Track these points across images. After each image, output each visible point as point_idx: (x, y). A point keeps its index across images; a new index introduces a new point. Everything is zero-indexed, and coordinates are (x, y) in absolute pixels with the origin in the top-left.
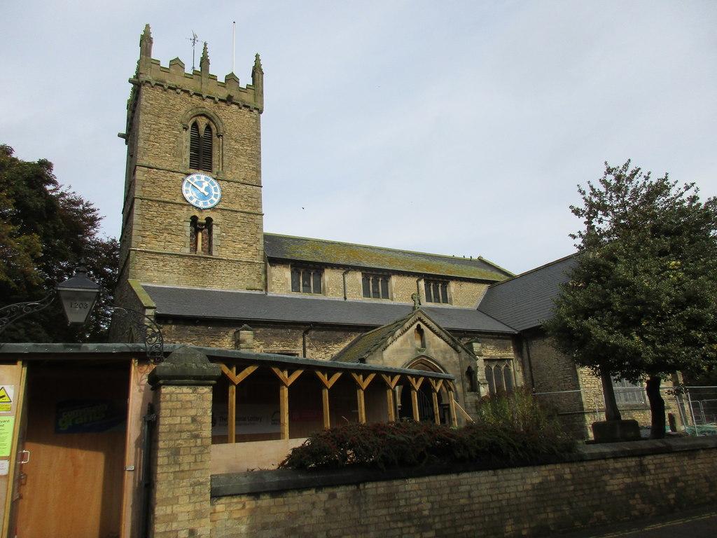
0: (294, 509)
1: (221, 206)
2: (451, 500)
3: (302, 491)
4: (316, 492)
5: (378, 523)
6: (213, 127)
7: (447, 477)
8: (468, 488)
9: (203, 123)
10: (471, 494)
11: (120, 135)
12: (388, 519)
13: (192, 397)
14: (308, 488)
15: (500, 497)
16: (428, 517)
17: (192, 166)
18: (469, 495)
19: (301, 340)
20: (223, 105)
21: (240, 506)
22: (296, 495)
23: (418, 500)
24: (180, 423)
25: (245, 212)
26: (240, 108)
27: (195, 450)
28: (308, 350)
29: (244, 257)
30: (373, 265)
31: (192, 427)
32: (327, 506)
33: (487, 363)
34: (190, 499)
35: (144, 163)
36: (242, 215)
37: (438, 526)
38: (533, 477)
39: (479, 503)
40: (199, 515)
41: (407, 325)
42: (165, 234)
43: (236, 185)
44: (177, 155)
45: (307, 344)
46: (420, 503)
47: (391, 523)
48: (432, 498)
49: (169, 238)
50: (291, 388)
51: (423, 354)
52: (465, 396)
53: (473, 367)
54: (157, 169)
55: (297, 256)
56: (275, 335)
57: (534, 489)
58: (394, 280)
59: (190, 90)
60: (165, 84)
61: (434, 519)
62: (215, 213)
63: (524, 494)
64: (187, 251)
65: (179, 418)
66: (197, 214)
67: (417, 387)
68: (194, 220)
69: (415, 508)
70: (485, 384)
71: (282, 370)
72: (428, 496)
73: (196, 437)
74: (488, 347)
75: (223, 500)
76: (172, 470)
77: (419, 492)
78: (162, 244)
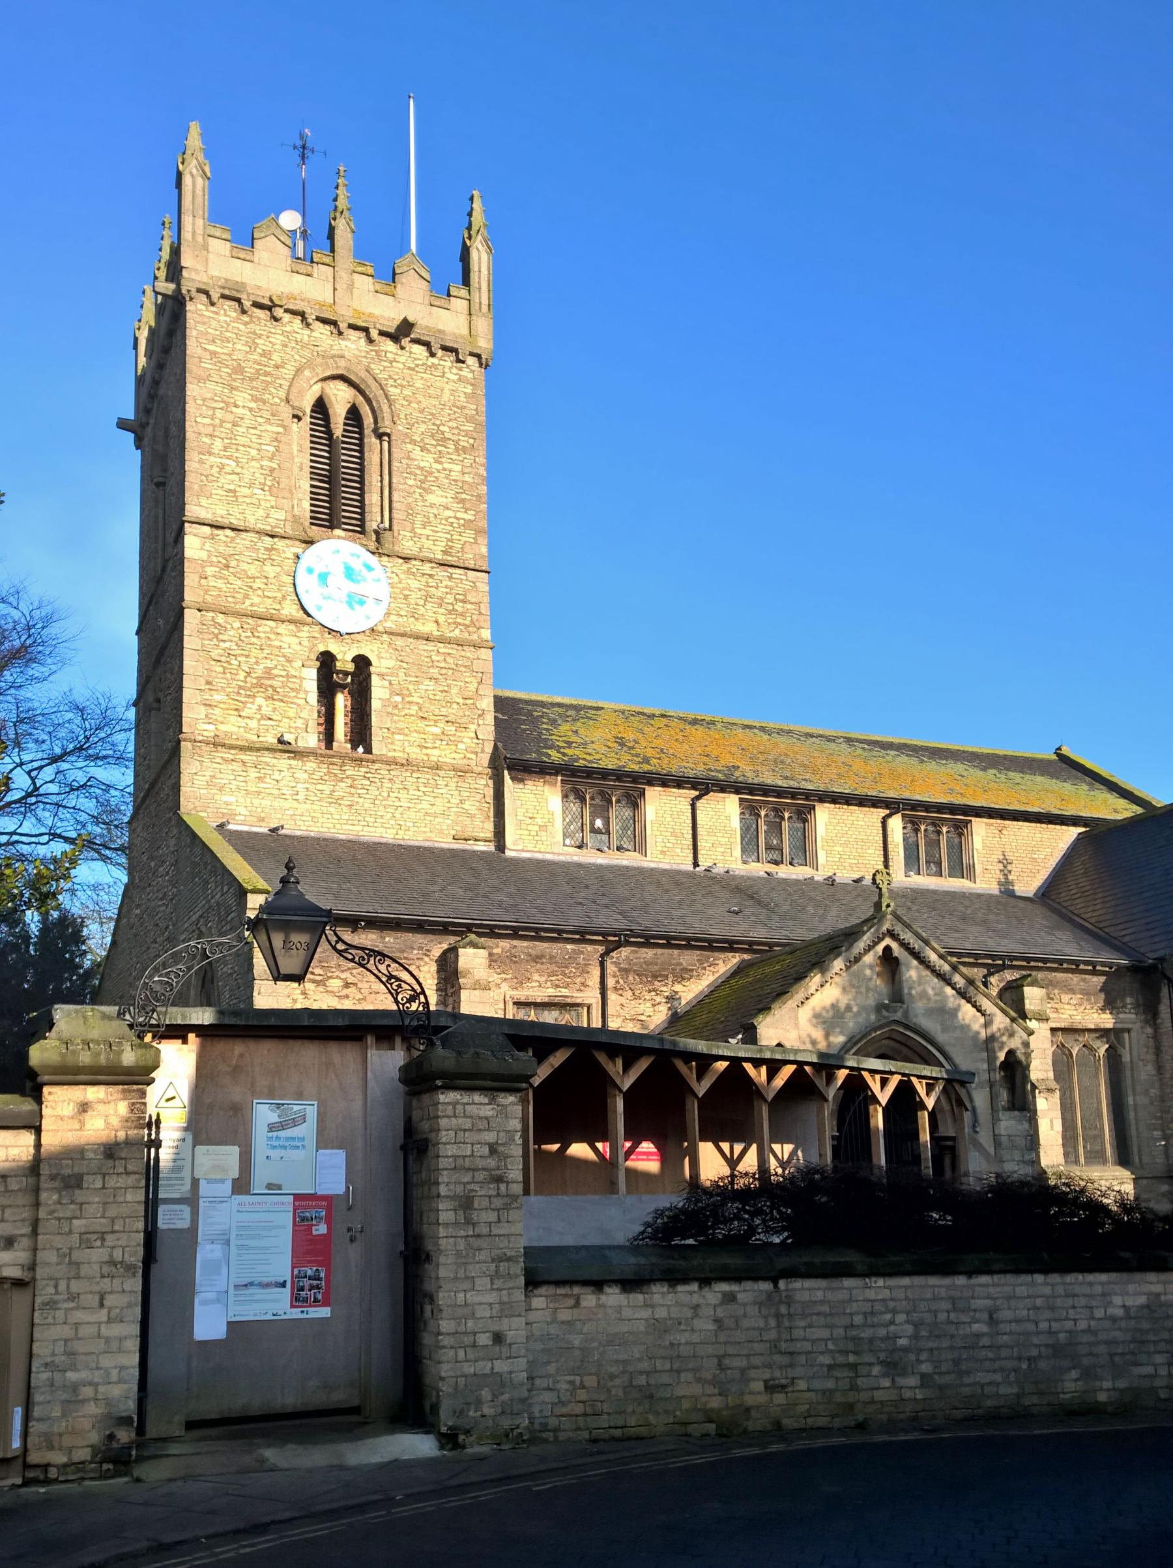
0: (661, 1313)
1: (389, 625)
2: (952, 1323)
3: (675, 1285)
4: (700, 1288)
5: (811, 1353)
6: (365, 410)
7: (947, 1281)
8: (988, 1303)
9: (340, 398)
10: (995, 1316)
11: (123, 424)
12: (831, 1346)
13: (488, 1111)
14: (686, 1280)
15: (1056, 1326)
16: (906, 1350)
17: (315, 520)
18: (991, 1317)
19: (596, 972)
20: (389, 346)
21: (572, 1302)
22: (665, 1289)
23: (888, 1316)
24: (472, 1156)
25: (449, 642)
26: (433, 355)
27: (498, 1203)
28: (612, 997)
29: (445, 755)
30: (769, 778)
31: (492, 1163)
32: (720, 1313)
33: (1060, 1037)
34: (492, 1283)
35: (204, 515)
36: (442, 648)
37: (925, 1368)
38: (1127, 1294)
39: (1011, 1333)
40: (506, 1310)
41: (861, 944)
42: (260, 701)
43: (427, 568)
44: (275, 485)
45: (610, 982)
46: (892, 1322)
47: (837, 1355)
48: (915, 1316)
49: (266, 710)
50: (629, 1096)
51: (898, 1016)
52: (995, 1120)
53: (1020, 1054)
54: (233, 529)
55: (582, 757)
56: (537, 959)
57: (1128, 1317)
58: (823, 815)
59: (308, 311)
60: (243, 296)
61: (918, 1355)
62: (375, 646)
63: (1107, 1324)
64: (312, 740)
65: (469, 1146)
66: (334, 647)
67: (884, 1097)
68: (327, 661)
69: (882, 1332)
70: (1050, 1090)
71: (612, 1057)
72: (908, 1313)
73: (499, 1180)
74: (1065, 998)
75: (543, 1290)
76: (462, 1233)
77: (891, 1304)
78: (253, 724)
